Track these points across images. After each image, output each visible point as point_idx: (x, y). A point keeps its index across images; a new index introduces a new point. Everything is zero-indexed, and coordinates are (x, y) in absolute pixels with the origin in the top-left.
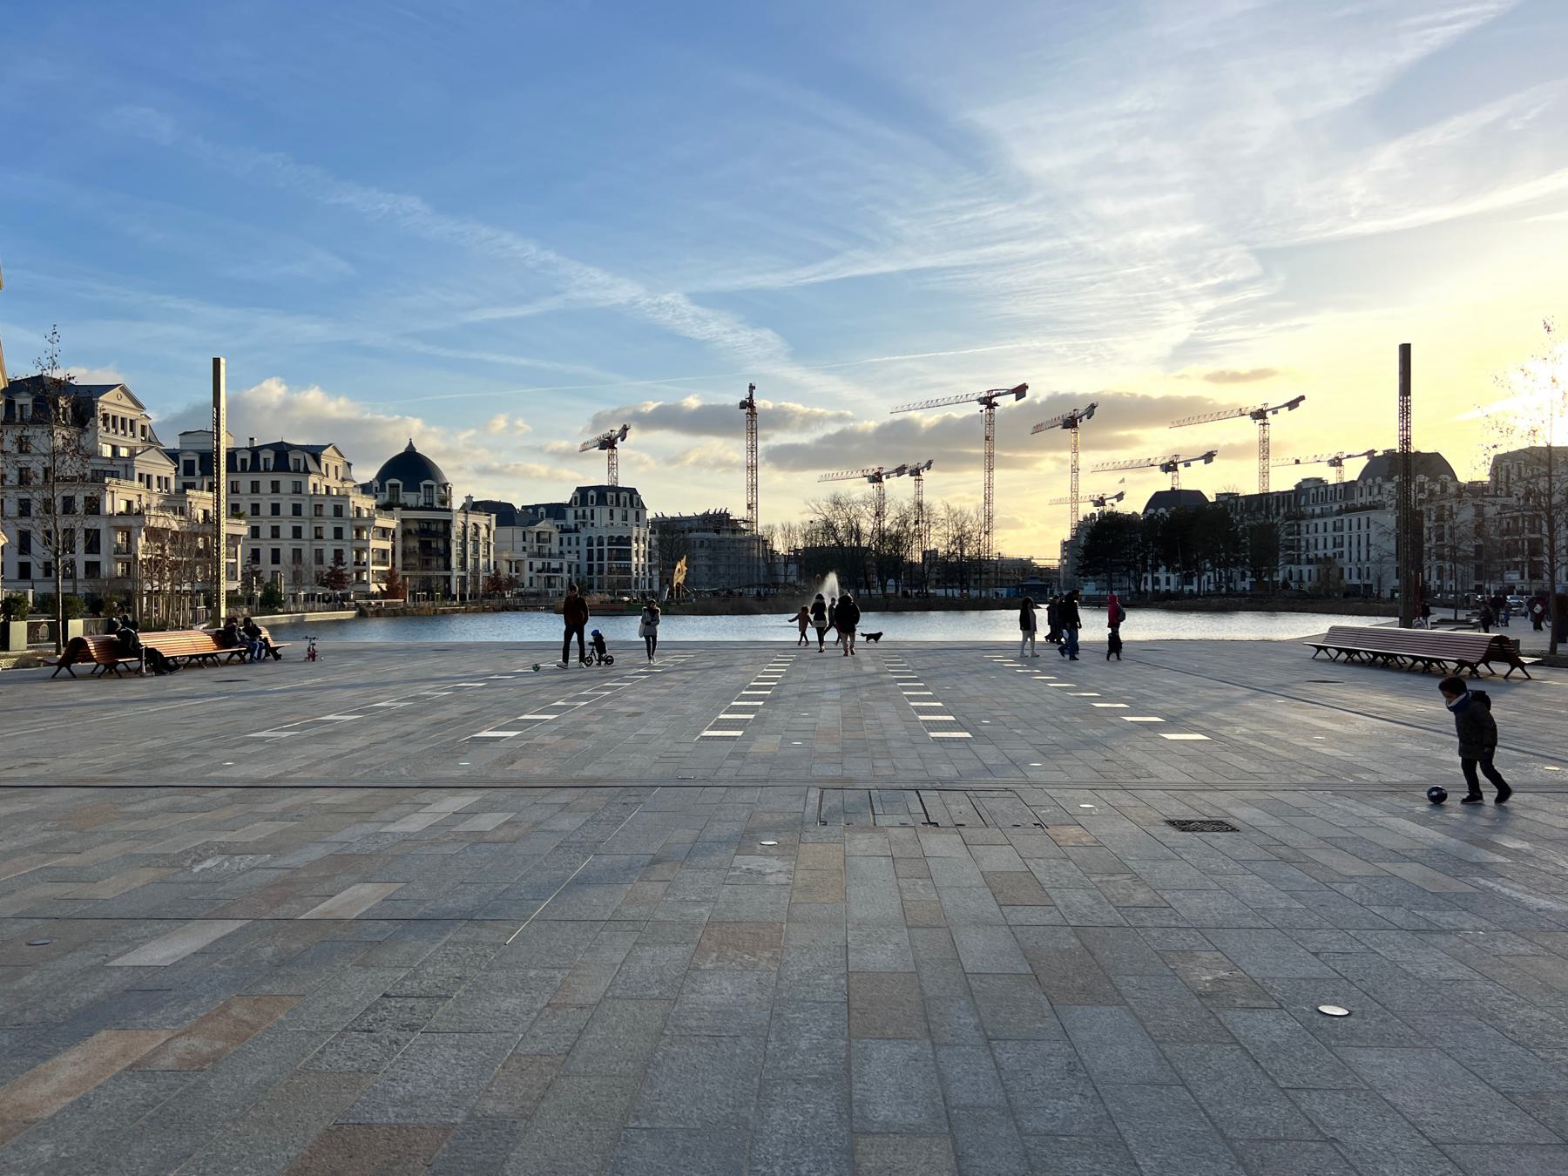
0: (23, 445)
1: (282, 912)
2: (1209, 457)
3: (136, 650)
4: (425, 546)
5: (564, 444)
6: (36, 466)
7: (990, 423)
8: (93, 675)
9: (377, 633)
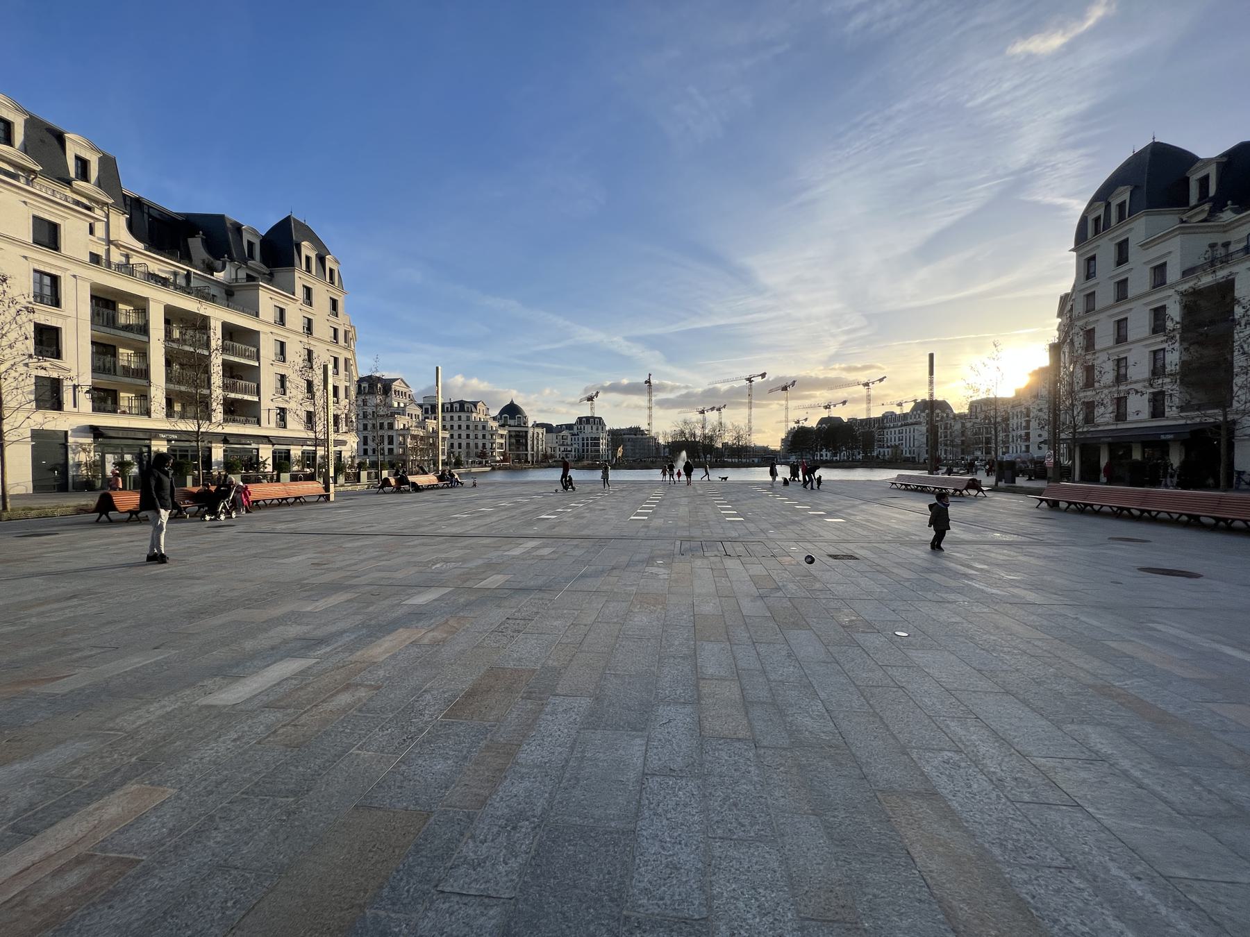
0: (365, 402)
1: (467, 585)
2: (844, 403)
3: (407, 483)
4: (518, 441)
5: (573, 400)
6: (370, 411)
7: (750, 388)
8: (392, 492)
9: (499, 477)
